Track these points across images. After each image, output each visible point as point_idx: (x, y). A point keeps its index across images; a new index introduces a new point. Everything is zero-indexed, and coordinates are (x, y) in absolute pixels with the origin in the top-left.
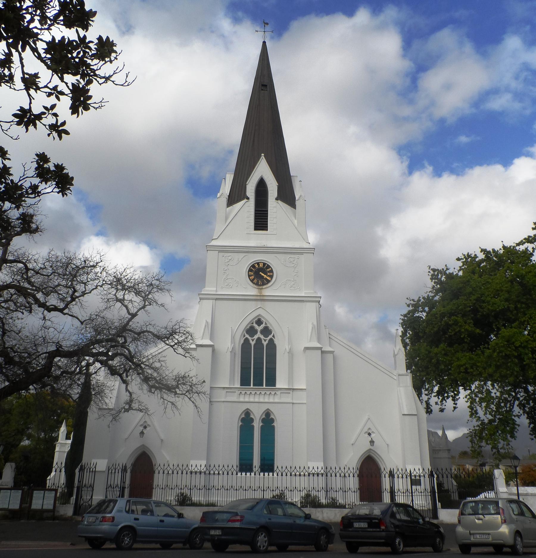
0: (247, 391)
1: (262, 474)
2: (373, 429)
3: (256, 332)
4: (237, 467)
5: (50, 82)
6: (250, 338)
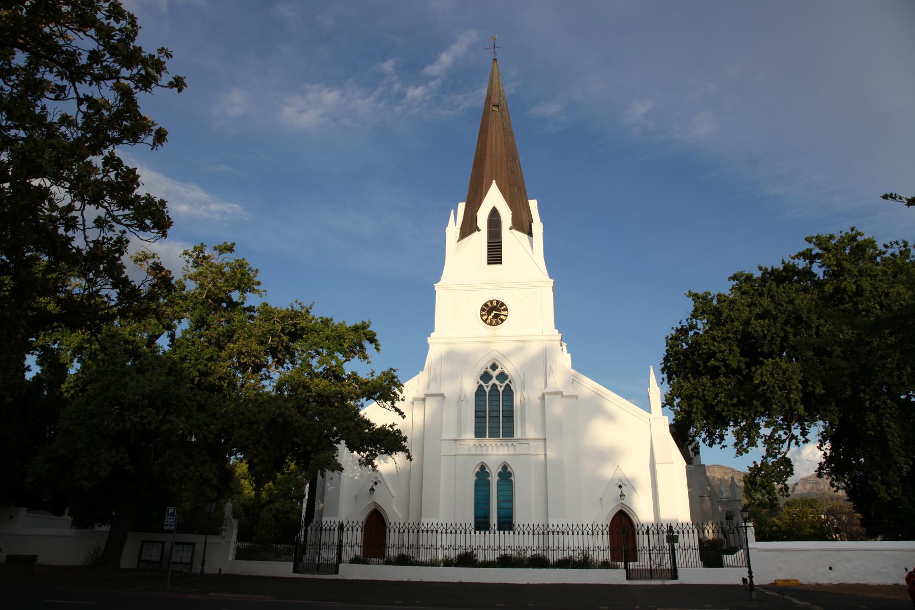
0: (502, 443)
1: (502, 532)
3: (491, 377)
5: (149, 144)
6: (484, 385)
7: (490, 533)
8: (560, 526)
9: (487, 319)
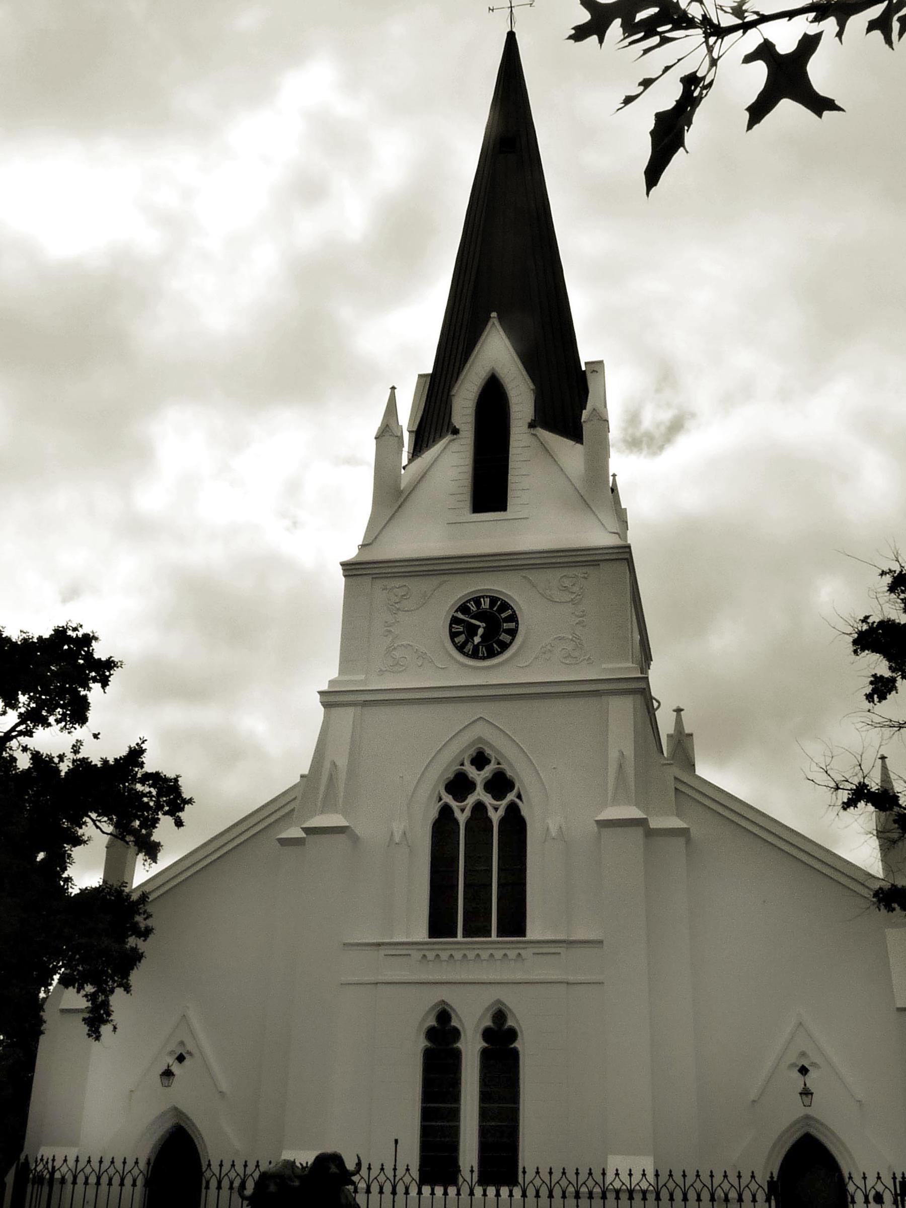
0: (453, 953)
2: (814, 1057)
4: (472, 1171)
6: (454, 804)
7: (458, 1194)
8: (624, 1177)
9: (465, 643)
